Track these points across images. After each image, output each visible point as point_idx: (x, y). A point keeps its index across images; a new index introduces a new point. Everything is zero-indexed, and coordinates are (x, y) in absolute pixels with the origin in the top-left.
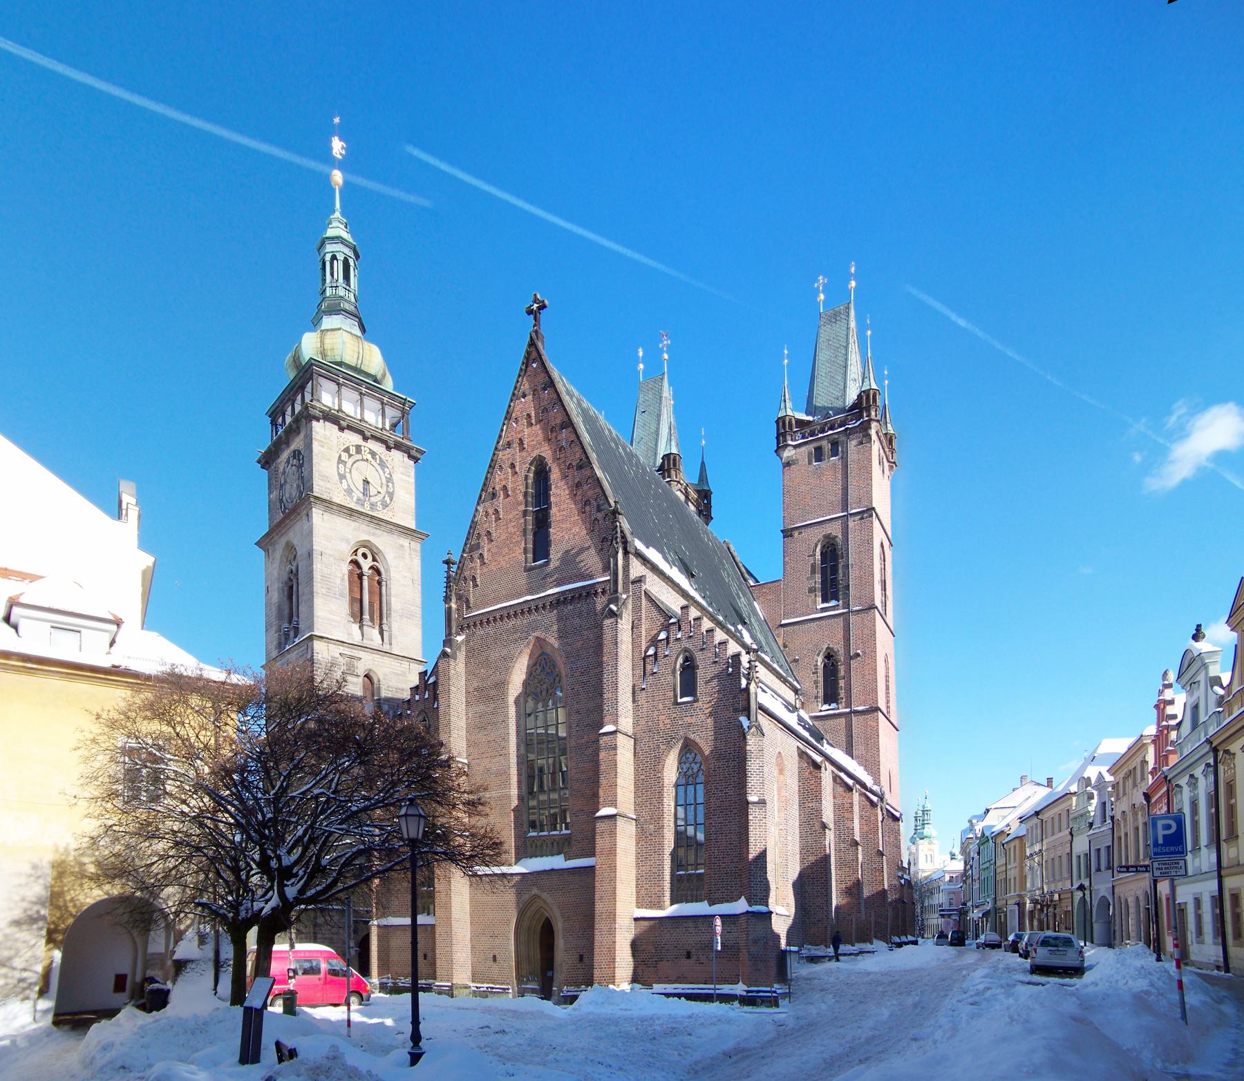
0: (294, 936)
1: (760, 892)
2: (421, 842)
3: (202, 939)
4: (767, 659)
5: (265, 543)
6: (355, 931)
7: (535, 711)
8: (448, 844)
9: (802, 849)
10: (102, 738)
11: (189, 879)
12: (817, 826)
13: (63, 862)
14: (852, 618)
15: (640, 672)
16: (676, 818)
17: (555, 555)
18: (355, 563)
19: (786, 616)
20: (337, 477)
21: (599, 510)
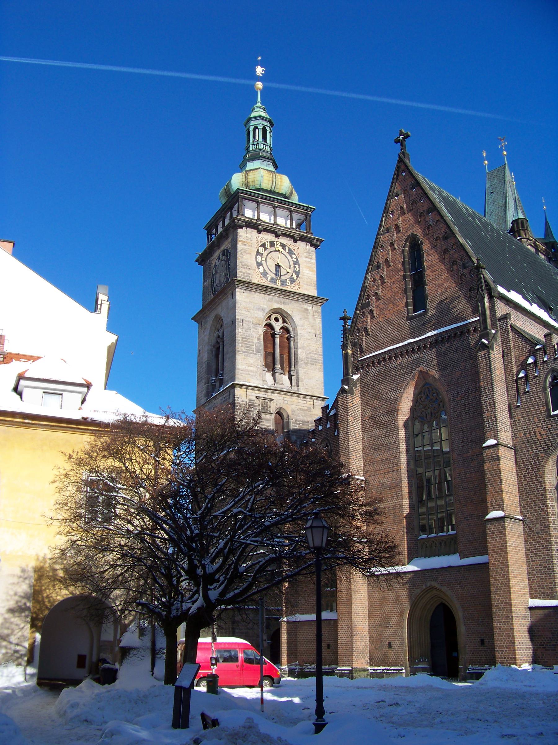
0: (215, 630)
2: (325, 549)
3: (142, 631)
5: (199, 318)
6: (268, 627)
7: (421, 432)
8: (349, 550)
10: (71, 473)
11: (132, 583)
13: (42, 568)
15: (513, 392)
17: (431, 306)
20: (256, 265)
21: (464, 267)
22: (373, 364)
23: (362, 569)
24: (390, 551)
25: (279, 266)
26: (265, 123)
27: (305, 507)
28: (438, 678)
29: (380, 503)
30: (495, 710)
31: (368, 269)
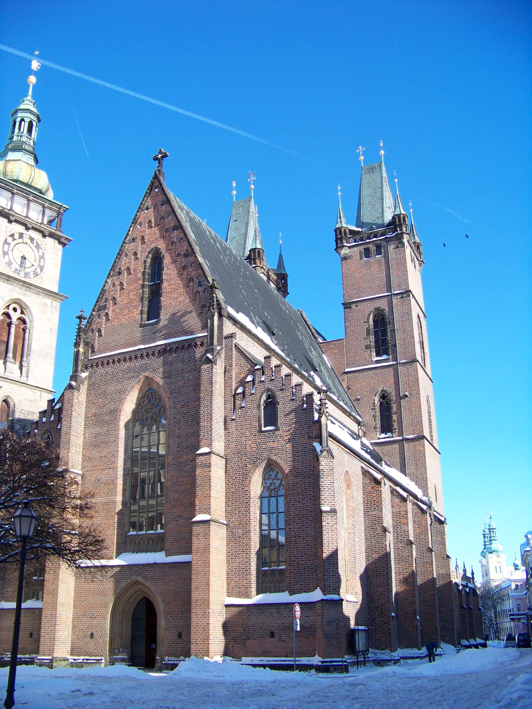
1: (332, 583)
4: (335, 398)
9: (367, 548)
12: (379, 530)
14: (400, 369)
15: (230, 406)
16: (261, 524)
17: (164, 316)
18: (7, 315)
19: (349, 366)
21: (200, 285)
22: (102, 364)
23: (69, 560)
24: (96, 545)
25: (25, 258)
26: (32, 117)
27: (18, 495)
28: (135, 668)
29: (91, 498)
30: (183, 698)
31: (110, 274)
